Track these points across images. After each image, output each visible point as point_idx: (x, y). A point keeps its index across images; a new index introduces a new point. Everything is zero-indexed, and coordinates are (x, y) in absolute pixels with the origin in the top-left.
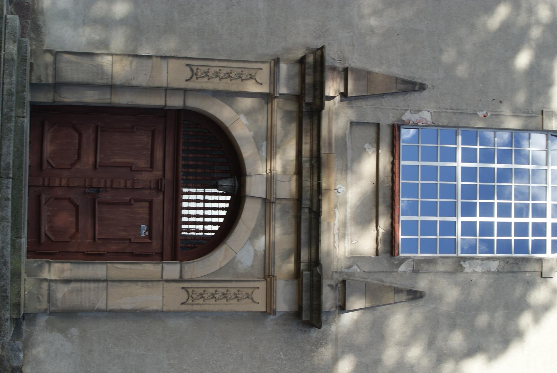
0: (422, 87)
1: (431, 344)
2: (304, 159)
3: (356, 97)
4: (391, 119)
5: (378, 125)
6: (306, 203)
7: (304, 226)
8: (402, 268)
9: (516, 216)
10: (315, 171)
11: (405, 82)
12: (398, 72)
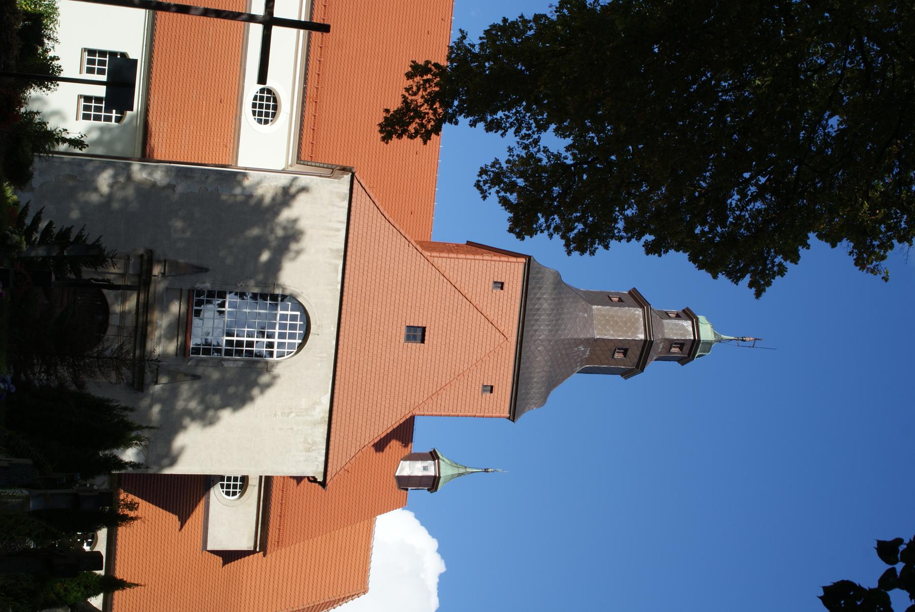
0: (207, 270)
1: (202, 401)
2: (140, 307)
3: (310, 107)
4: (189, 287)
5: (181, 290)
6: (140, 329)
7: (138, 339)
8: (189, 363)
9: (279, 333)
10: (145, 314)
11: (197, 267)
12: (194, 262)
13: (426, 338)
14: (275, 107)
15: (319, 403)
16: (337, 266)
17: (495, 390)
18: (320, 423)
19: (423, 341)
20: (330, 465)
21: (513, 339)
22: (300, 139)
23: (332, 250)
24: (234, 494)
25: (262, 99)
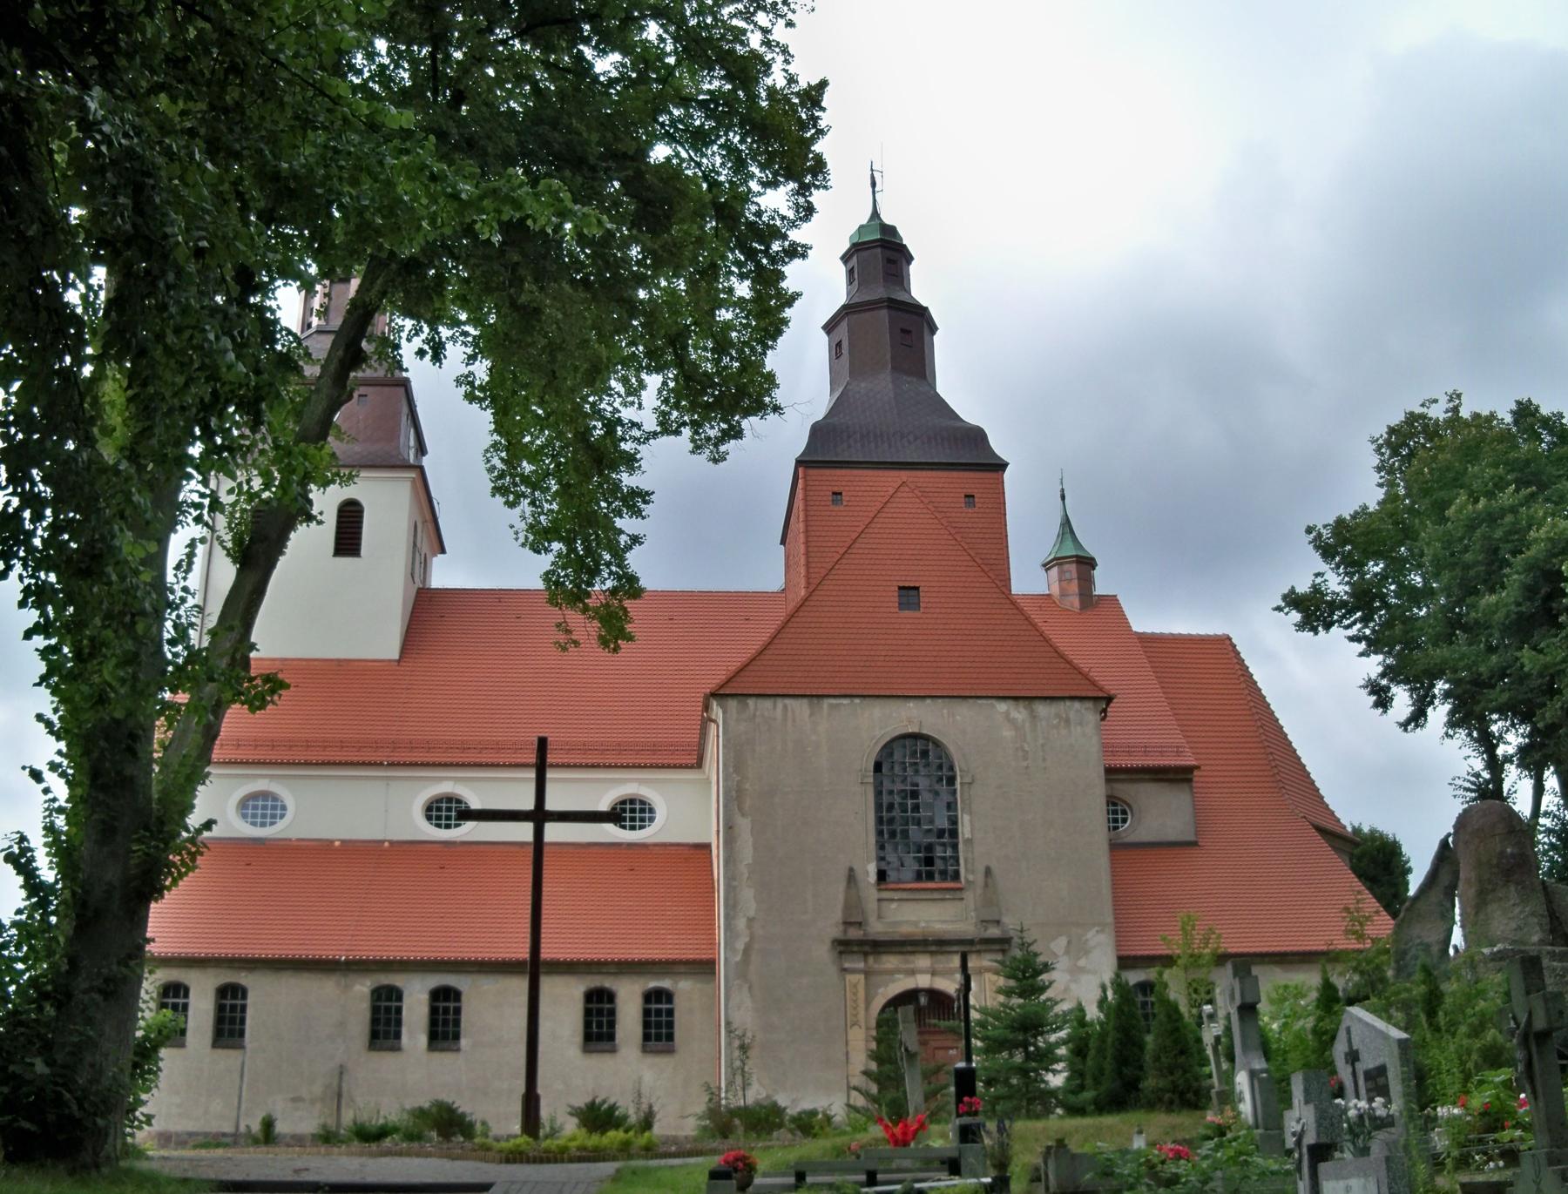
13: (912, 585)
14: (632, 801)
15: (1007, 714)
16: (831, 706)
17: (969, 492)
18: (1032, 711)
19: (917, 588)
20: (1084, 694)
21: (904, 475)
22: (669, 767)
23: (811, 715)
24: (1124, 812)
25: (254, 816)
